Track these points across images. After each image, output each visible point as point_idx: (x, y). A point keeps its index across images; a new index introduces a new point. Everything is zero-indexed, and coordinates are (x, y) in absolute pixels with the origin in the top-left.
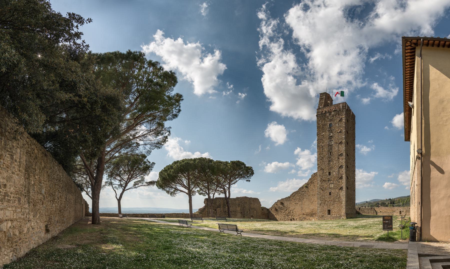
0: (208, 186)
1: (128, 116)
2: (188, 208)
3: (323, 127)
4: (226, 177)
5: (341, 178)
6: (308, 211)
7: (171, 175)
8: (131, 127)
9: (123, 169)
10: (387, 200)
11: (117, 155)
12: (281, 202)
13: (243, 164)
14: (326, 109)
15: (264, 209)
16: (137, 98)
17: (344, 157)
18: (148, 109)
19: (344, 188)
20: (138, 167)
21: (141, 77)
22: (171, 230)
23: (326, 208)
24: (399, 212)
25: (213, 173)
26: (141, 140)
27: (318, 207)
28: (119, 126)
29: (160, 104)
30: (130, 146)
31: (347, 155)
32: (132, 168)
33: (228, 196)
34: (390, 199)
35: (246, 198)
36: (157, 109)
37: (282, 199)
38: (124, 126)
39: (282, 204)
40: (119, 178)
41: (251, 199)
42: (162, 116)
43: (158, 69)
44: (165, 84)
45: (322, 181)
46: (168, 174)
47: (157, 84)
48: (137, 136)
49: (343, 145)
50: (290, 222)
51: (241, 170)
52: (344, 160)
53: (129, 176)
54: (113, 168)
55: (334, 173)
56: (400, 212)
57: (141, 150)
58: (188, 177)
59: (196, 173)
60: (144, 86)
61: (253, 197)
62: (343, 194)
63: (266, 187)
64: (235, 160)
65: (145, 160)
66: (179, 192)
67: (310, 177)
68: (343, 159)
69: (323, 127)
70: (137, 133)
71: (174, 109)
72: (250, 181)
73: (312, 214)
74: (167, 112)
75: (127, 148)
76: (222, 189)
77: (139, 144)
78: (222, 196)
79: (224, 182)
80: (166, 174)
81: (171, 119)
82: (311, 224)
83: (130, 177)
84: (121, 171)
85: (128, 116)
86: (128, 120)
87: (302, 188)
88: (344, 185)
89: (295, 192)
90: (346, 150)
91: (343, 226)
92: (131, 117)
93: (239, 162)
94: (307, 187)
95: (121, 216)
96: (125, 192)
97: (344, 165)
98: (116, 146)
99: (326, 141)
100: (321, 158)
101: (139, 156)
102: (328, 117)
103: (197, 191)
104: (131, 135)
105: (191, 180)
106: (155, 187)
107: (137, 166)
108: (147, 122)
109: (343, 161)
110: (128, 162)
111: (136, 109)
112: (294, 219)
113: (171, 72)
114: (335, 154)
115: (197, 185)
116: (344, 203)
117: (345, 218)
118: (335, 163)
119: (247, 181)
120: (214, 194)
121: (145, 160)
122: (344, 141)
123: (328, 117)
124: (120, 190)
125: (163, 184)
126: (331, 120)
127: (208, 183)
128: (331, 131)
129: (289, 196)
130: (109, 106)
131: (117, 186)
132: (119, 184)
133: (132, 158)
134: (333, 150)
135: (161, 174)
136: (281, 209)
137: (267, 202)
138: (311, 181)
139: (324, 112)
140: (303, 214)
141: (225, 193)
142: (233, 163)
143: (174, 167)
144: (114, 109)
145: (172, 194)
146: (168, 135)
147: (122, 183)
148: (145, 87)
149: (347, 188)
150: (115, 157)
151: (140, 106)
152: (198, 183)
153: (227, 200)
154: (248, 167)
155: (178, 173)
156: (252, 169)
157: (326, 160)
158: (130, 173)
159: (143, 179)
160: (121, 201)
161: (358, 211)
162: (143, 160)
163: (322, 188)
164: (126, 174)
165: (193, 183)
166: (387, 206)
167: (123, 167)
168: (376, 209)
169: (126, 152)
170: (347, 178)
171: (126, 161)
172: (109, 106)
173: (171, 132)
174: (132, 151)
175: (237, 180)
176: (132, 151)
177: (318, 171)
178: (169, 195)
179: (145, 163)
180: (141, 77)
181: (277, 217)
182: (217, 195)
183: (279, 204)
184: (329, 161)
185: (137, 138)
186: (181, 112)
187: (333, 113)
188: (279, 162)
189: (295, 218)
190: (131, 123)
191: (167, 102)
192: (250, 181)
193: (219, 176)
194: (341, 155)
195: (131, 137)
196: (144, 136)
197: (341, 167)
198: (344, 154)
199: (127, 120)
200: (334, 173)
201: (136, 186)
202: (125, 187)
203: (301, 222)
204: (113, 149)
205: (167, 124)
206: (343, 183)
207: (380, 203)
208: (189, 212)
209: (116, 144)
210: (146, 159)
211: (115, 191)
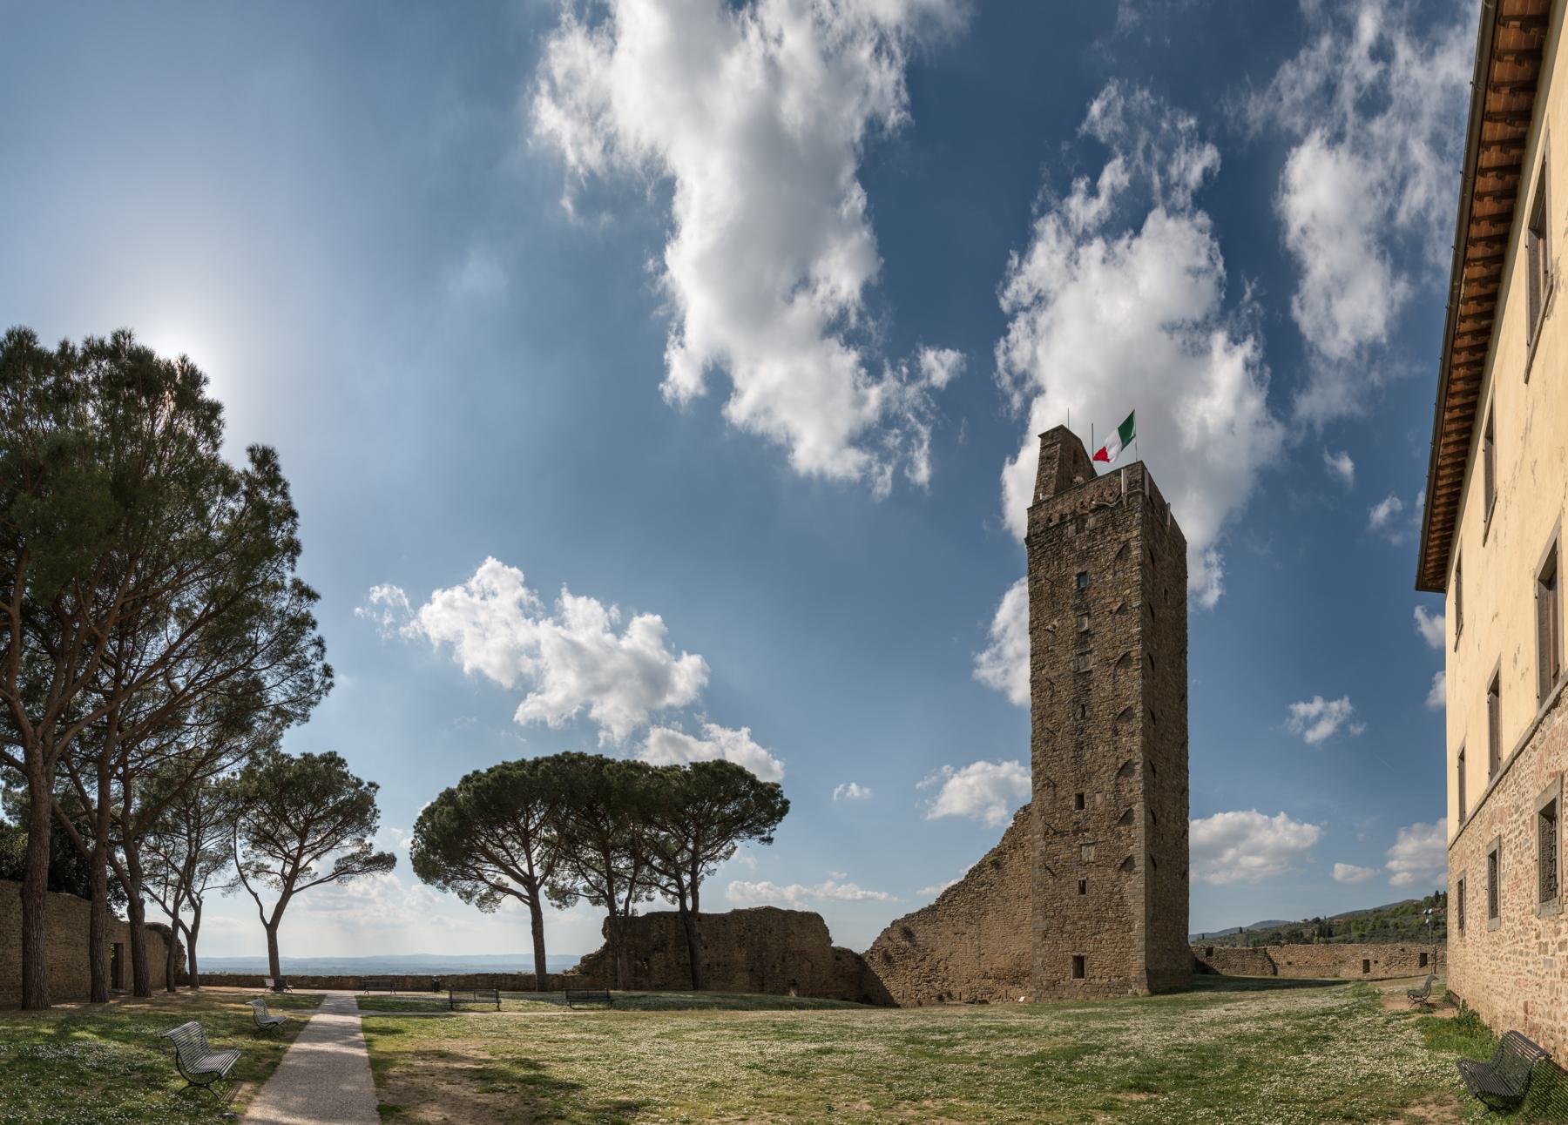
2: (530, 949)
3: (1053, 594)
5: (1127, 818)
6: (1001, 962)
10: (1306, 924)
12: (905, 928)
14: (1064, 506)
17: (1137, 724)
19: (1140, 864)
23: (1067, 951)
24: (1360, 966)
27: (1035, 946)
31: (1151, 716)
33: (689, 904)
34: (1317, 920)
37: (908, 917)
39: (908, 934)
41: (790, 915)
45: (1052, 833)
49: (1135, 671)
52: (1138, 739)
55: (1099, 798)
56: (1366, 963)
61: (799, 907)
62: (1135, 887)
68: (1133, 734)
69: (1053, 594)
73: (1017, 976)
87: (979, 869)
90: (1146, 693)
94: (996, 865)
97: (1138, 758)
99: (1067, 657)
102: (1071, 541)
109: (1132, 744)
112: (949, 995)
114: (1102, 711)
116: (1138, 925)
117: (1142, 991)
122: (1136, 650)
123: (1071, 541)
126: (1084, 556)
128: (1083, 609)
129: (933, 903)
134: (1095, 697)
137: (854, 932)
138: (1014, 839)
139: (1056, 521)
140: (986, 976)
149: (1153, 862)
153: (688, 922)
157: (1065, 741)
160: (279, 931)
161: (1203, 959)
163: (1049, 863)
166: (1308, 942)
168: (1273, 951)
170: (1153, 818)
178: (473, 906)
181: (893, 986)
183: (896, 935)
184: (1079, 746)
187: (1091, 522)
189: (955, 991)
194: (1127, 715)
197: (1125, 770)
198: (1138, 711)
200: (1099, 798)
206: (1136, 841)
207: (1284, 933)
208: (532, 970)
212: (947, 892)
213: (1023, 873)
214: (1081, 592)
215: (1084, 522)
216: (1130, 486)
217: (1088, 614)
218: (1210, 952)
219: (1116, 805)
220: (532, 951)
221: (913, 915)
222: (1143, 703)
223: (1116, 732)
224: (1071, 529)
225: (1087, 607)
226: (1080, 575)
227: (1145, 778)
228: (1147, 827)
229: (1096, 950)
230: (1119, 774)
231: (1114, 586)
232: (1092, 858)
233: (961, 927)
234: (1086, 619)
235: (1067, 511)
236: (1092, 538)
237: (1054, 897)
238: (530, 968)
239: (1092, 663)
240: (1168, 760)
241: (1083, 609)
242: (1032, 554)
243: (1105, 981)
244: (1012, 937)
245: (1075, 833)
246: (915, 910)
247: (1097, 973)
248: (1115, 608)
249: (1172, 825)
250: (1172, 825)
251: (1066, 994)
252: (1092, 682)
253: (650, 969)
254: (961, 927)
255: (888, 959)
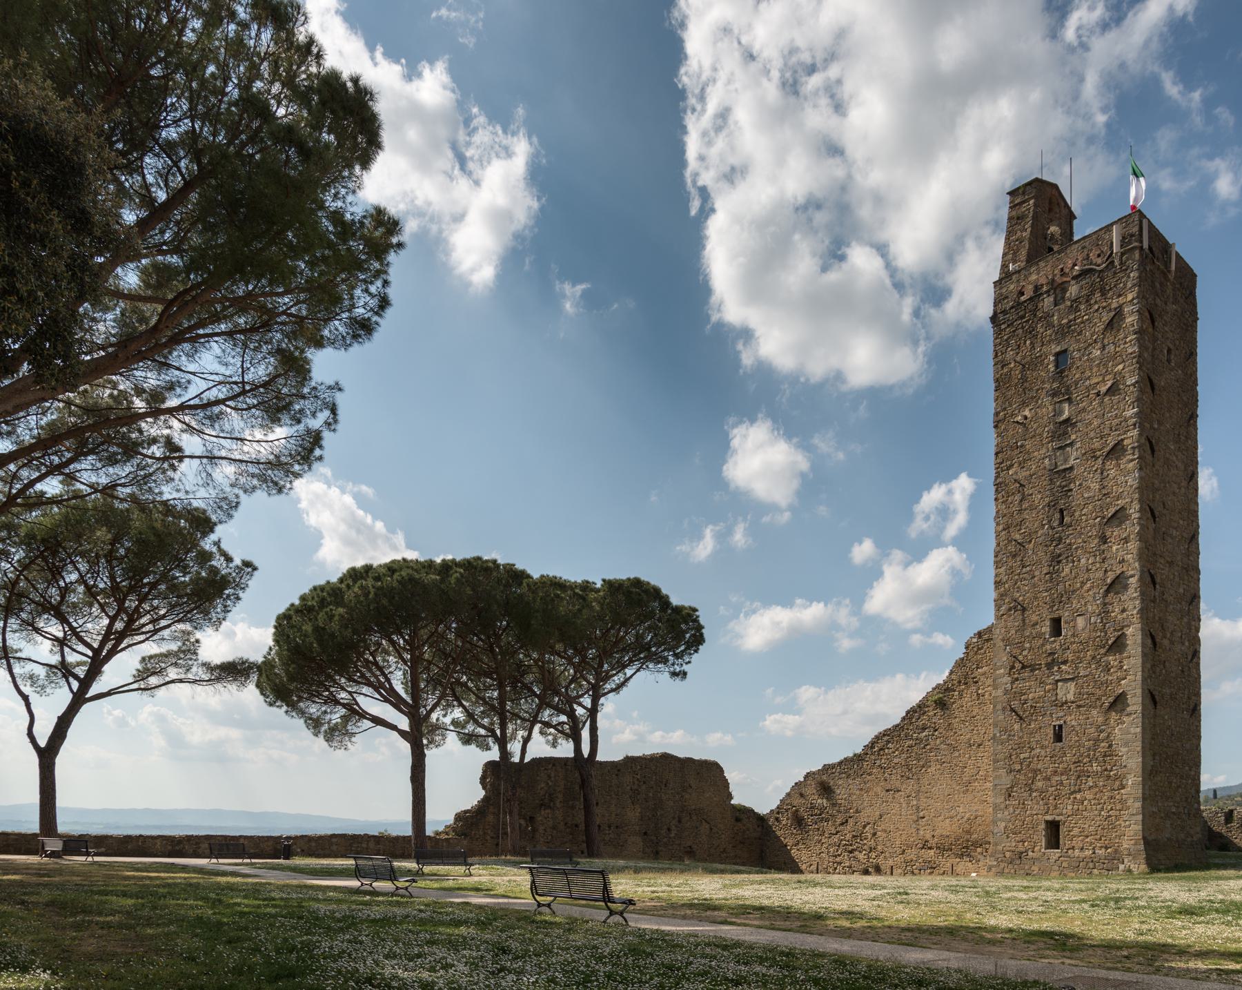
0: (502, 699)
1: (129, 278)
2: (408, 817)
3: (1024, 379)
4: (584, 658)
5: (1118, 645)
6: (946, 828)
7: (332, 635)
8: (146, 344)
9: (82, 580)
11: (52, 487)
12: (822, 782)
13: (656, 593)
14: (1041, 274)
15: (745, 813)
16: (188, 186)
17: (1132, 527)
18: (240, 267)
19: (1135, 703)
20: (164, 577)
21: (212, 69)
22: (315, 905)
23: (1038, 814)
25: (527, 638)
26: (189, 429)
28: (75, 318)
29: (295, 252)
30: (131, 450)
31: (1151, 513)
32: (136, 574)
33: (586, 750)
35: (666, 757)
36: (281, 276)
37: (827, 768)
38: (105, 325)
39: (826, 790)
40: (56, 630)
42: (302, 319)
43: (299, 48)
44: (327, 145)
45: (1020, 667)
46: (317, 629)
47: (287, 135)
48: (172, 402)
49: (1130, 463)
50: (857, 878)
51: (644, 625)
52: (1133, 546)
53: (113, 620)
54: (25, 566)
55: (1081, 622)
57: (186, 485)
58: (412, 651)
59: (452, 636)
60: (224, 125)
62: (1128, 732)
63: (762, 707)
64: (622, 572)
65: (207, 544)
66: (367, 724)
67: (960, 653)
68: (1126, 540)
69: (1024, 379)
70: (171, 387)
71: (358, 292)
72: (685, 674)
73: (966, 847)
74: (326, 299)
75: (112, 461)
76: (563, 718)
77: (179, 449)
78: (565, 749)
79: (574, 680)
80: (308, 628)
81: (343, 343)
82: (954, 890)
83: (119, 625)
84: (65, 591)
85: (129, 278)
86: (130, 297)
88: (1133, 685)
89: (885, 733)
91: (1117, 900)
92: (147, 285)
93: (637, 582)
95: (53, 845)
96: (86, 708)
98: (49, 440)
99: (1041, 455)
100: (1011, 548)
101: (179, 516)
102: (1048, 316)
103: (455, 723)
104: (139, 391)
105: (427, 669)
106: (249, 695)
107: (159, 568)
108: (230, 334)
109: (1126, 552)
110: (116, 540)
111: (176, 250)
113: (355, 80)
114: (1086, 515)
115: (452, 693)
116: (1133, 782)
117: (1139, 866)
118: (1085, 569)
119: (674, 674)
120: (526, 741)
121: (207, 544)
122: (1132, 437)
123: (1048, 316)
124: (61, 697)
125: (292, 678)
126: (1064, 332)
127: (501, 687)
128: (1063, 394)
129: (859, 750)
130: (26, 184)
131: (41, 672)
132: (55, 659)
133: (137, 521)
134: (1077, 499)
135: (285, 625)
136: (821, 815)
137: (758, 788)
138: (965, 672)
140: (925, 846)
141: (576, 737)
142: (613, 587)
143: (349, 596)
144: (54, 215)
145: (336, 734)
146: (328, 424)
147: (72, 658)
148: (233, 134)
149: (1152, 698)
150: (41, 501)
151: (196, 239)
152: (458, 682)
154: (678, 610)
155: (369, 630)
156: (696, 621)
157: (1037, 555)
158: (121, 602)
159: (189, 650)
161: (1218, 826)
162: (195, 544)
163: (1015, 704)
164: (96, 610)
165: (434, 682)
167: (83, 567)
169: (104, 480)
170: (1152, 640)
171: (102, 533)
172: (26, 184)
173: (340, 412)
174: (142, 480)
175: (629, 672)
176: (142, 480)
177: (998, 617)
178: (321, 738)
179: (205, 557)
180: (212, 69)
182: (540, 747)
183: (811, 790)
184: (1056, 559)
185: (171, 411)
186: (389, 313)
187: (1073, 290)
188: (787, 603)
190: (143, 319)
191: (331, 245)
192: (685, 674)
193: (554, 652)
195: (139, 404)
196: (207, 409)
197: (1116, 585)
198: (1134, 512)
199: (118, 294)
200: (1081, 622)
201: (153, 680)
202: (86, 683)
203: (904, 881)
204: (31, 448)
205: (325, 364)
208: (408, 831)
209: (51, 424)
210: (213, 537)
211: (25, 698)
212: (878, 738)
213: (982, 713)
214: (1060, 372)
215: (1064, 290)
216: (1124, 241)
217: (1069, 400)
218: (1229, 816)
219: (1103, 630)
220: (34, 798)
221: (832, 766)
222: (1141, 501)
223: (1104, 539)
224: (1048, 301)
225: (1068, 392)
226: (1057, 355)
227: (1142, 594)
228: (1144, 655)
229: (1076, 812)
230: (1107, 591)
231: (1103, 362)
232: (1070, 697)
233: (895, 781)
234: (1066, 405)
235: (1043, 281)
236: (1074, 308)
237: (1020, 746)
238: (31, 823)
239: (1073, 457)
240: (1171, 563)
241: (1063, 394)
242: (998, 333)
243: (1088, 853)
244: (967, 792)
245: (1049, 666)
246: (836, 760)
247: (1077, 842)
248: (1104, 389)
249: (1177, 648)
250: (1177, 648)
251: (1035, 868)
252: (1073, 480)
253: (534, 830)
254: (895, 781)
255: (799, 821)
